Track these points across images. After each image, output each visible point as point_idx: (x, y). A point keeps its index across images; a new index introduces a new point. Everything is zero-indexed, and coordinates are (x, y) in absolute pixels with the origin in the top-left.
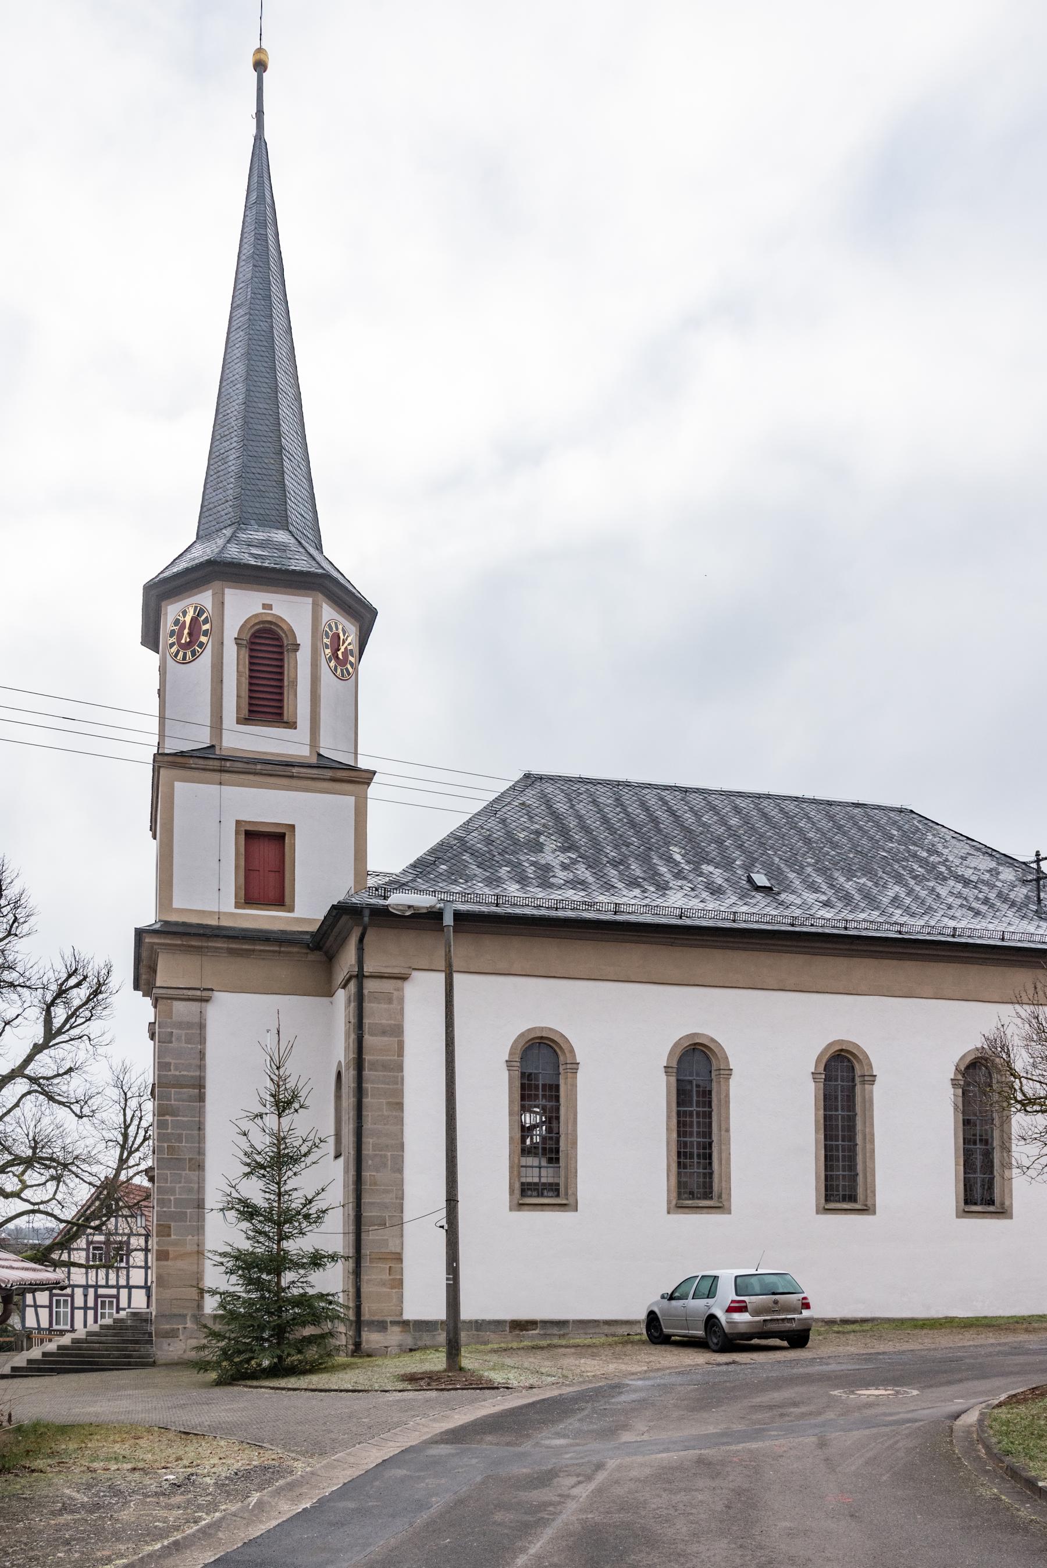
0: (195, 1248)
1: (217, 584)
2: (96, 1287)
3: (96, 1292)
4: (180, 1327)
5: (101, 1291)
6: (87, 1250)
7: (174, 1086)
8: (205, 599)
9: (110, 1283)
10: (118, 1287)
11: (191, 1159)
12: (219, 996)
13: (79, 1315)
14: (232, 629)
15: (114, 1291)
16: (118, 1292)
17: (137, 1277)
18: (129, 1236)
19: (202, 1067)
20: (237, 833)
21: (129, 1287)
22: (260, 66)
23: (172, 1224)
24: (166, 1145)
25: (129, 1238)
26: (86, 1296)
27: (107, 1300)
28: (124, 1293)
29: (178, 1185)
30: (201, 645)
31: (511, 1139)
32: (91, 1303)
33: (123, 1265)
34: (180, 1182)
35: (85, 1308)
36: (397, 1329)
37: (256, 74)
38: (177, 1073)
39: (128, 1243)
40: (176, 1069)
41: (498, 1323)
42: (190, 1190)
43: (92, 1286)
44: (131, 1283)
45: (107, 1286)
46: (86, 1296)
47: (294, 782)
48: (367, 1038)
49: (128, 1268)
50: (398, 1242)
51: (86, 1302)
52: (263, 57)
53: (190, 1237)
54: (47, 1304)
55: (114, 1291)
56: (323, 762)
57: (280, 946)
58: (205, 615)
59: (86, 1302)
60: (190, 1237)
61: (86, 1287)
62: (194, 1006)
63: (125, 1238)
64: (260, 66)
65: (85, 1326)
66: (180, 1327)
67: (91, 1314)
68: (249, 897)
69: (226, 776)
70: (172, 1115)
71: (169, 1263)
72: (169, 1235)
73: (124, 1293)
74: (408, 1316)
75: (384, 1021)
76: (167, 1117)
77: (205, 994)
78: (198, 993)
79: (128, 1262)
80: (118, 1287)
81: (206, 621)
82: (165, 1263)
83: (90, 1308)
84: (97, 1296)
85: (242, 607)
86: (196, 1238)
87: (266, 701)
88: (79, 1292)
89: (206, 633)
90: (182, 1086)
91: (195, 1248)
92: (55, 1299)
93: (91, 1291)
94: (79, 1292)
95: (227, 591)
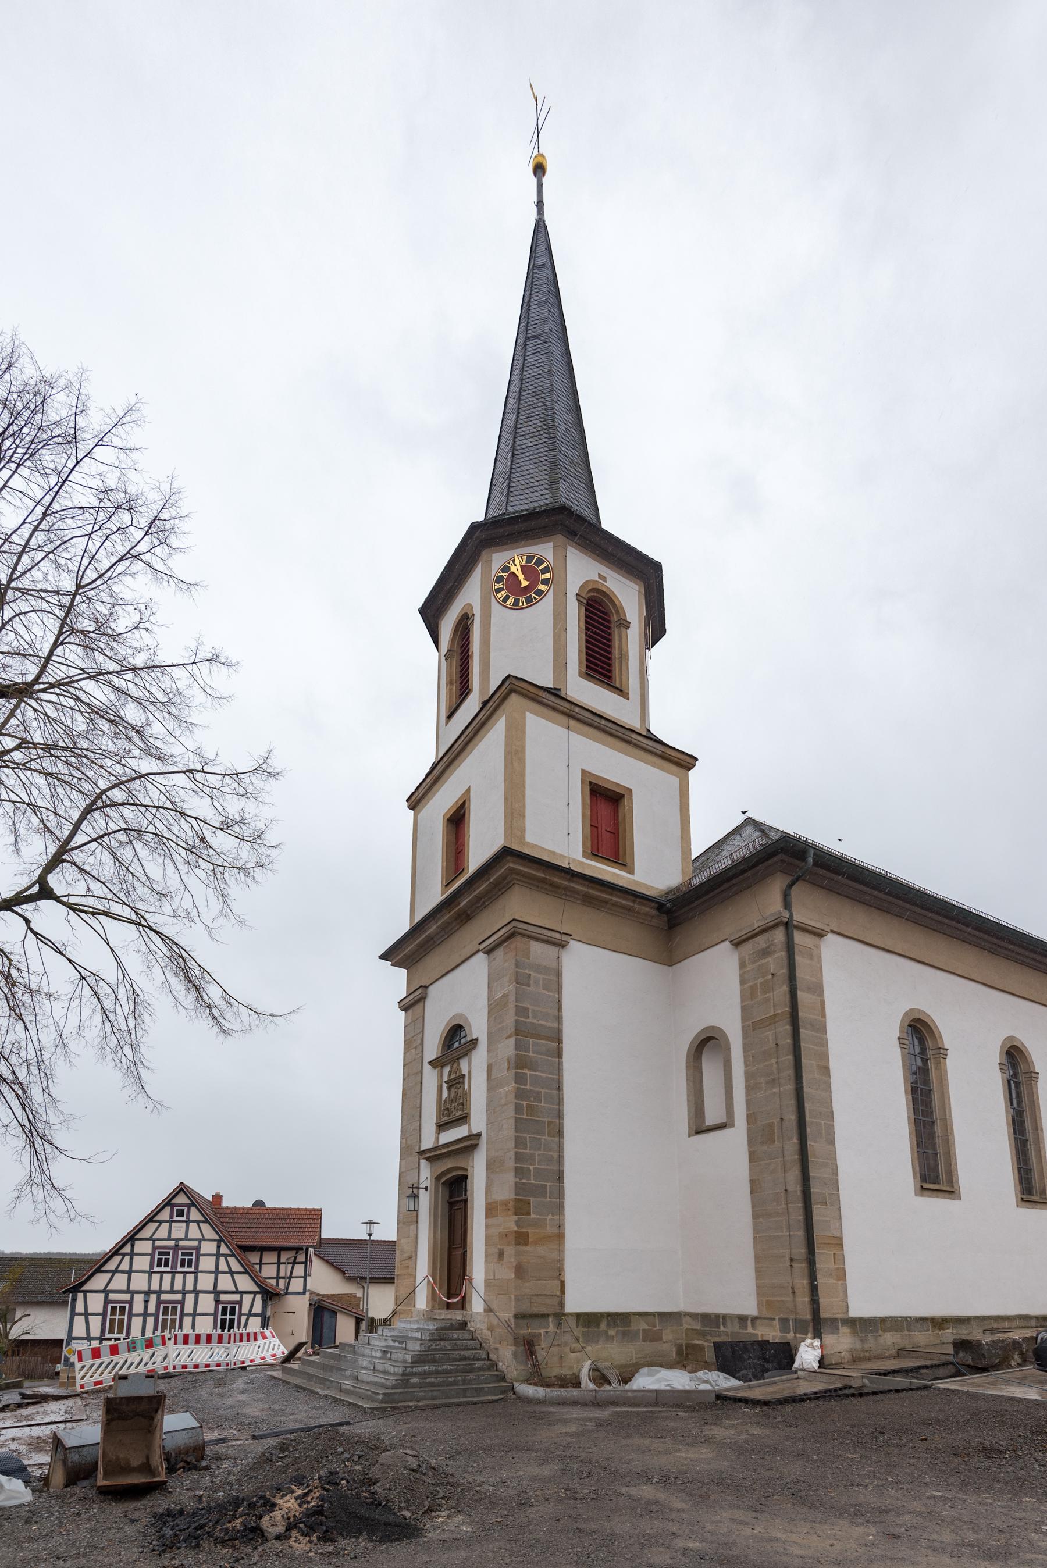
0: (556, 1231)
1: (560, 538)
2: (159, 1292)
3: (159, 1297)
4: (542, 1331)
5: (164, 1297)
6: (152, 1255)
7: (533, 1036)
8: (545, 550)
9: (176, 1288)
10: (184, 1292)
11: (550, 1123)
12: (575, 947)
13: (137, 1322)
14: (573, 587)
15: (179, 1297)
16: (184, 1298)
17: (206, 1282)
18: (200, 1241)
19: (559, 1019)
20: (583, 782)
21: (196, 1292)
22: (539, 169)
23: (532, 1199)
24: (524, 1103)
25: (200, 1243)
26: (146, 1302)
27: (170, 1306)
28: (190, 1299)
29: (537, 1153)
30: (540, 593)
31: (909, 1117)
32: (152, 1309)
33: (192, 1269)
34: (539, 1149)
35: (145, 1315)
36: (845, 1330)
37: (535, 180)
38: (535, 1021)
39: (198, 1249)
40: (534, 1017)
41: (923, 1319)
42: (550, 1159)
43: (154, 1292)
44: (199, 1288)
45: (172, 1291)
46: (146, 1302)
47: (630, 748)
48: (801, 995)
49: (196, 1273)
50: (838, 1224)
51: (146, 1308)
52: (541, 160)
53: (550, 1217)
54: (101, 1311)
55: (179, 1297)
56: (649, 735)
57: (634, 902)
58: (545, 565)
59: (146, 1308)
60: (550, 1217)
61: (148, 1293)
62: (551, 951)
63: (196, 1243)
64: (539, 169)
65: (143, 1333)
66: (542, 1331)
67: (150, 1320)
68: (594, 851)
69: (572, 722)
70: (531, 1069)
71: (528, 1248)
72: (529, 1214)
73: (190, 1299)
74: (853, 1313)
75: (808, 977)
76: (526, 1071)
77: (565, 938)
78: (558, 936)
79: (197, 1267)
80: (184, 1292)
81: (546, 570)
82: (525, 1248)
83: (151, 1315)
84: (159, 1302)
85: (581, 569)
86: (556, 1217)
87: (601, 661)
88: (139, 1299)
89: (546, 582)
90: (538, 1036)
91: (556, 1231)
92: (110, 1306)
93: (153, 1297)
94: (139, 1299)
95: (569, 548)
